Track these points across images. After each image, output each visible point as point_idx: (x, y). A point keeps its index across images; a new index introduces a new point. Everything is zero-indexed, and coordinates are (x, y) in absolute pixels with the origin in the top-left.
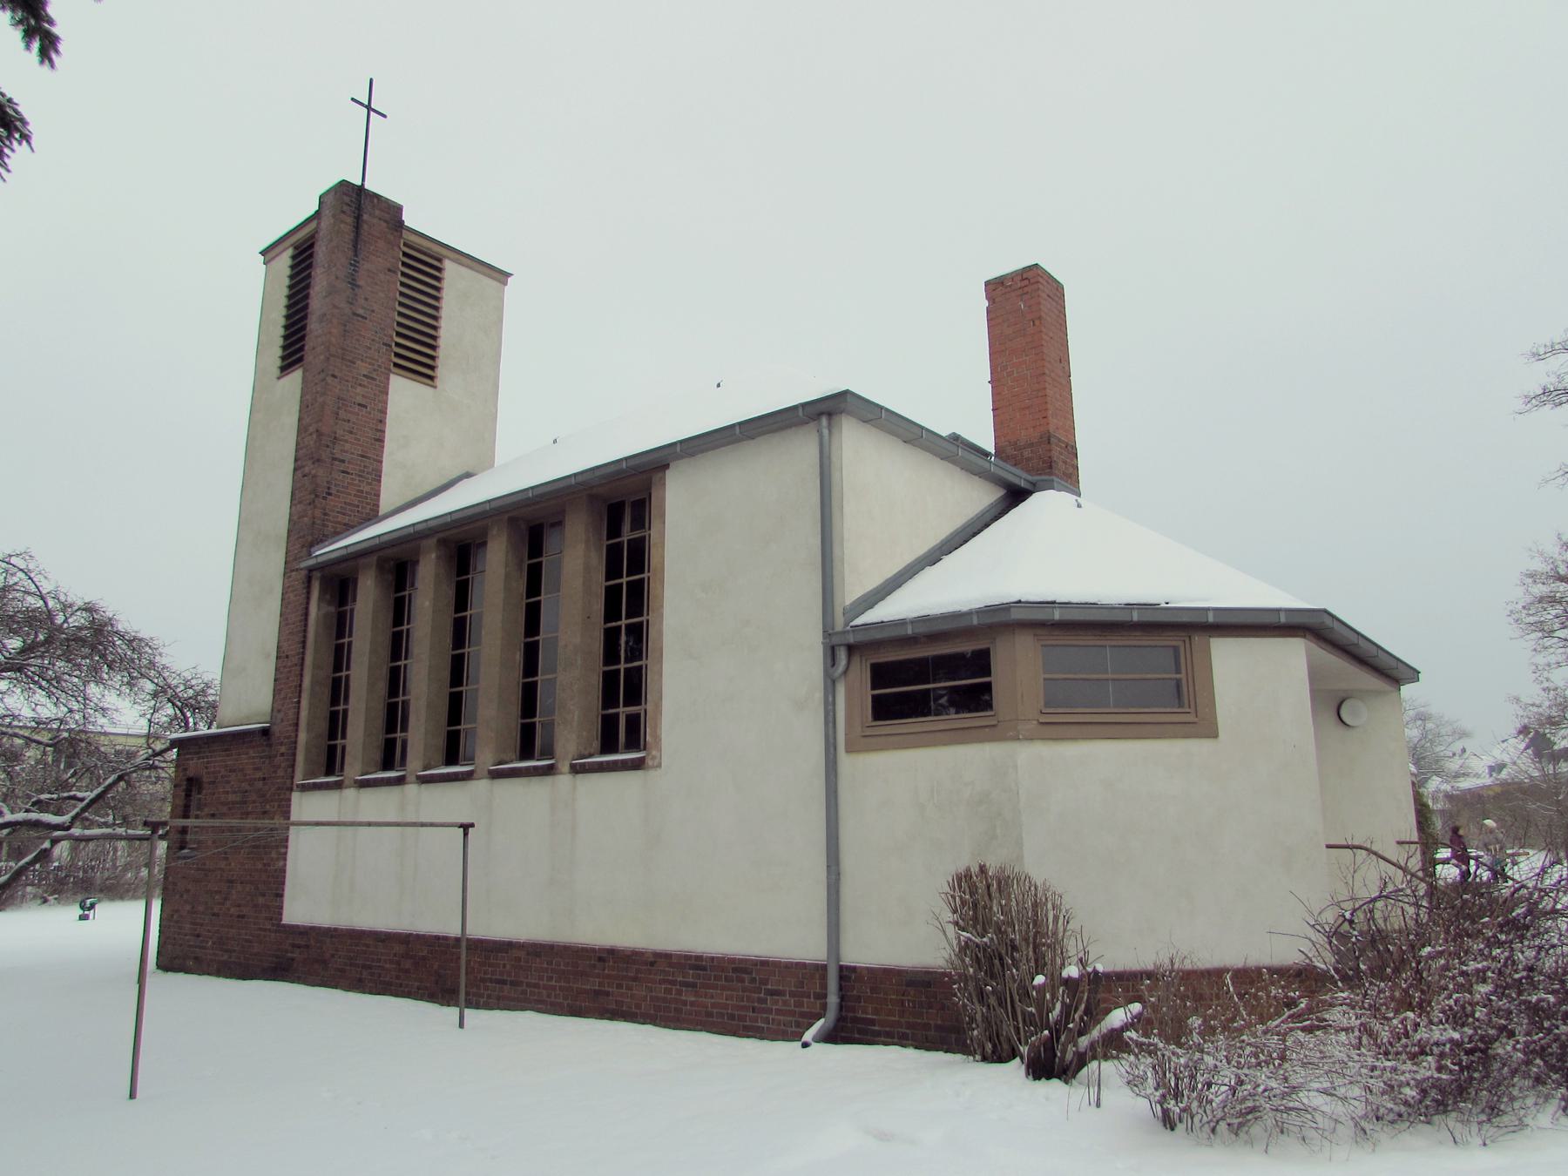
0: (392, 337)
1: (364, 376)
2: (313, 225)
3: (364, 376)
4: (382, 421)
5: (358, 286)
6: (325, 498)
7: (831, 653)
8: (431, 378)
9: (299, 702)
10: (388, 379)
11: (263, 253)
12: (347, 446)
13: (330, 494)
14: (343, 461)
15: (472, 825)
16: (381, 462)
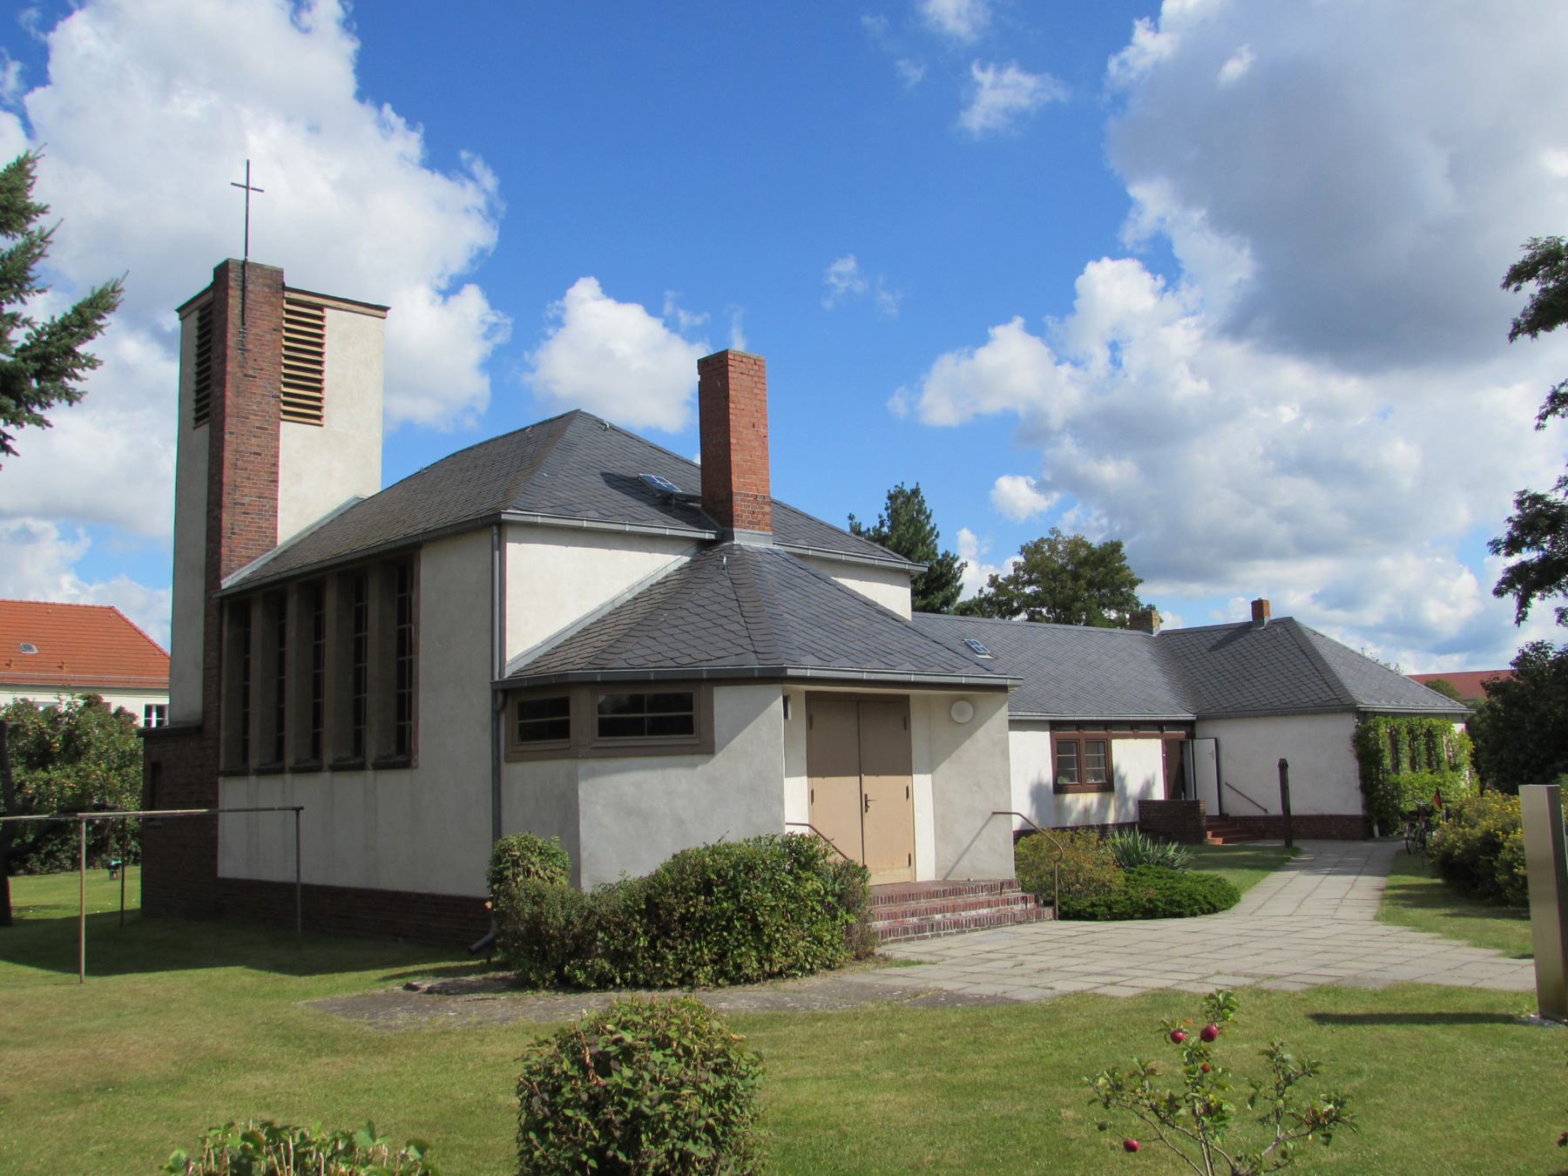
0: (280, 389)
1: (257, 428)
2: (211, 295)
3: (257, 428)
4: (276, 465)
5: (248, 351)
6: (230, 538)
7: (494, 692)
8: (319, 418)
9: (219, 706)
10: (279, 426)
11: (179, 310)
12: (247, 490)
13: (234, 533)
14: (243, 504)
15: (302, 808)
16: (276, 499)
